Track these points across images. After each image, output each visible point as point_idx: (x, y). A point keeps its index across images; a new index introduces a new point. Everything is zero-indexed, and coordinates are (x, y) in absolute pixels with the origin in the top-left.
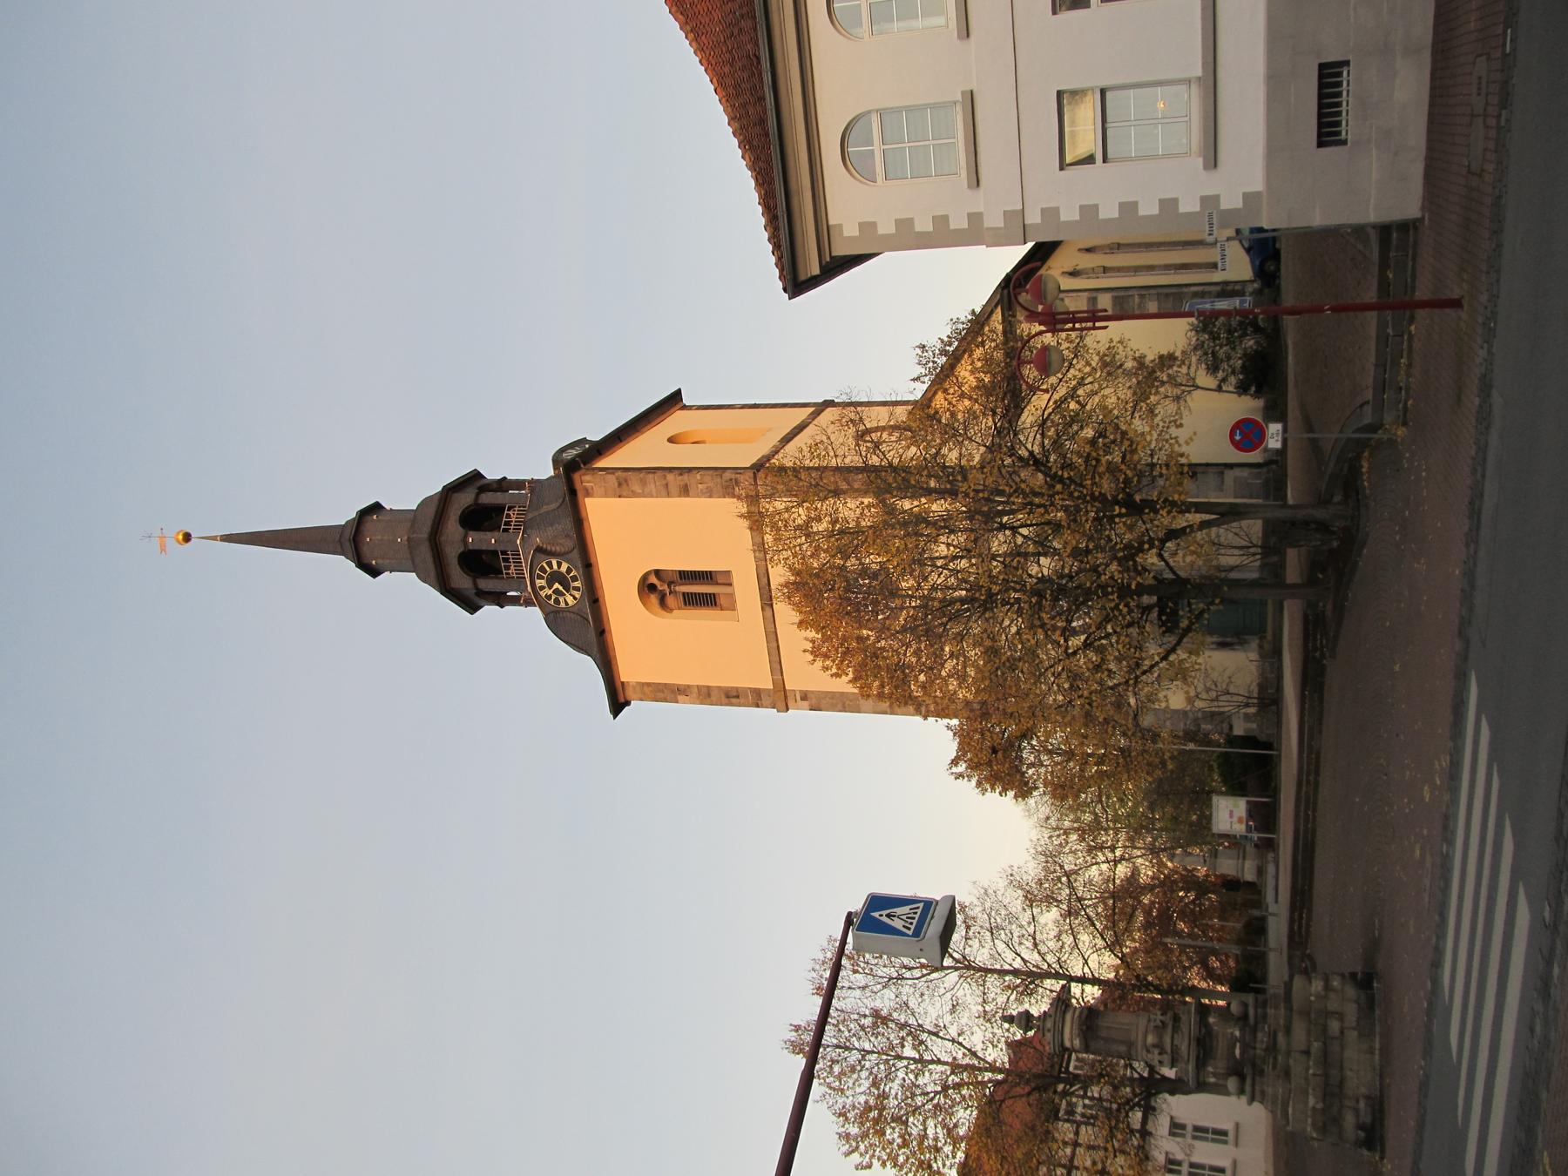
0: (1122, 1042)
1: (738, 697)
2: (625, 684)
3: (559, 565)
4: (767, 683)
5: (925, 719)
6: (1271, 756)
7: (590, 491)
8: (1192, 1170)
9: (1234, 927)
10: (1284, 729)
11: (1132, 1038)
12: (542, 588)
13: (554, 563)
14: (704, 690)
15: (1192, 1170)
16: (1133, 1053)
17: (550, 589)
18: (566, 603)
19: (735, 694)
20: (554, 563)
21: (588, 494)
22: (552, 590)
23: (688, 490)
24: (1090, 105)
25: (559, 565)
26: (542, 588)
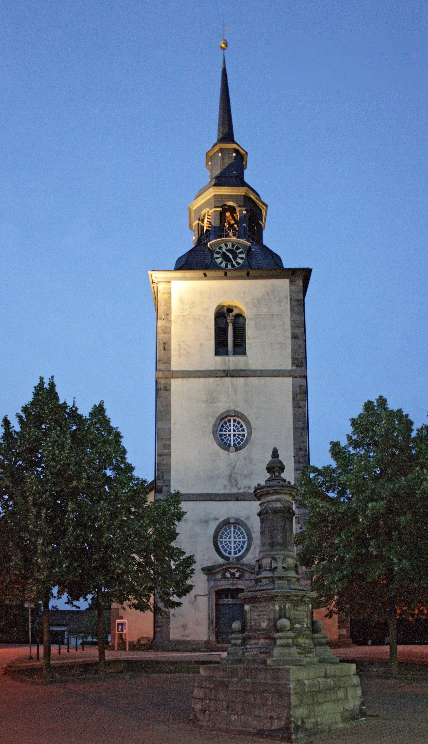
0: (285, 539)
1: (164, 349)
2: (170, 284)
3: (242, 258)
4: (175, 366)
5: (400, 411)
6: (129, 642)
7: (293, 283)
8: (30, 610)
9: (249, 633)
10: (4, 644)
11: (288, 547)
12: (226, 245)
13: (242, 256)
14: (168, 330)
15: (30, 610)
16: (277, 548)
17: (226, 250)
18: (217, 258)
19: (166, 348)
20: (242, 256)
21: (291, 282)
22: (225, 251)
23: (295, 338)
24: (222, 561)
25: (242, 258)
26: (226, 245)
